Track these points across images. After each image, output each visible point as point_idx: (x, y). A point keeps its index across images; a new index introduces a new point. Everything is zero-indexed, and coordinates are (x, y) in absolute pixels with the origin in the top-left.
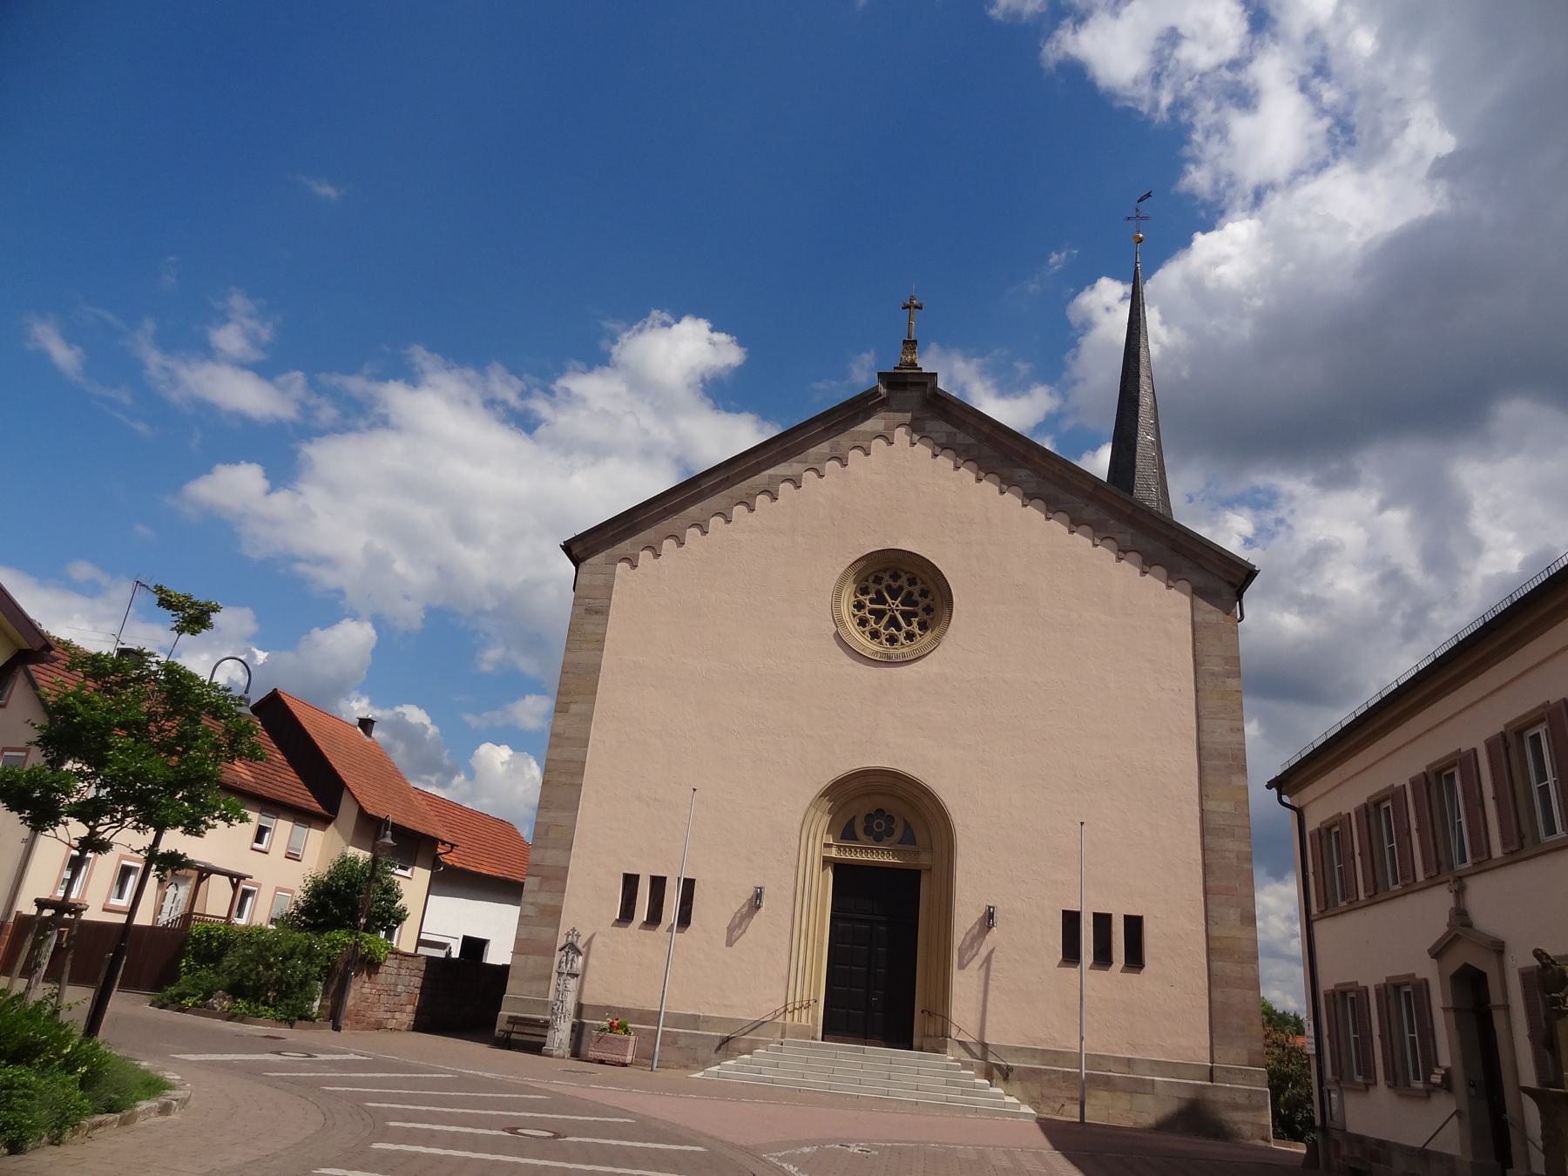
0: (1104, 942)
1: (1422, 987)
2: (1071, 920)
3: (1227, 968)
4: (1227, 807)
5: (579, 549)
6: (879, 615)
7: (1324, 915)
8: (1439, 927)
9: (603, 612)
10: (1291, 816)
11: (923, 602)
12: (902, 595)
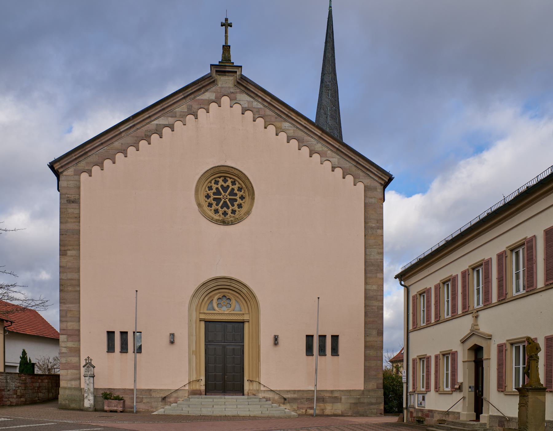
0: (321, 345)
1: (454, 354)
2: (309, 338)
3: (372, 353)
4: (375, 287)
5: (56, 167)
6: (218, 200)
7: (415, 329)
8: (466, 331)
9: (76, 201)
10: (402, 290)
11: (240, 194)
12: (226, 194)
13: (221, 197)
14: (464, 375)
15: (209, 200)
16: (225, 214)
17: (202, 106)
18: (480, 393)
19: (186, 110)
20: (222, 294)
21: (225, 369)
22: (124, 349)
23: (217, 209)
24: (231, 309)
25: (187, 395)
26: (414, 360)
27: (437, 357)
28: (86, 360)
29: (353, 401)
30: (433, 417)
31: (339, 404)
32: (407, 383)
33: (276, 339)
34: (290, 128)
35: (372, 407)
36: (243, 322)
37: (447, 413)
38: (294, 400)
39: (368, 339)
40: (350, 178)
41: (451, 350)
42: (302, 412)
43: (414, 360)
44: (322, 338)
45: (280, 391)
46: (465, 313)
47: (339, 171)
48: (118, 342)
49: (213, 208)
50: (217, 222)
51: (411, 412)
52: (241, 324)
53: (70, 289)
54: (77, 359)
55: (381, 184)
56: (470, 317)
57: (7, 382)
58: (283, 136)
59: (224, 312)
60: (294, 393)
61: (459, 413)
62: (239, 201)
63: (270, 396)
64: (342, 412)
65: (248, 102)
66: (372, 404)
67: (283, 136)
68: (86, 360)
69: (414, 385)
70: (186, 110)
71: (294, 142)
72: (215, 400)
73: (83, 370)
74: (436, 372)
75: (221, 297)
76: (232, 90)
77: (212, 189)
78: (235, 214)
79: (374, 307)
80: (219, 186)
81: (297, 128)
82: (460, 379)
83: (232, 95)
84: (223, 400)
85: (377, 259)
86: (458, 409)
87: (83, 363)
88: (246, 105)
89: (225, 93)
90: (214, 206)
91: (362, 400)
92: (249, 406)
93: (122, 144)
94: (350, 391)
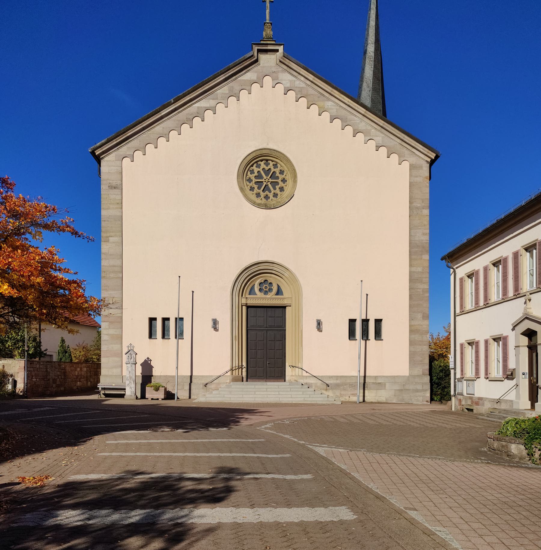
0: (363, 329)
7: (463, 313)
8: (519, 315)
13: (265, 184)
14: (519, 360)
15: (251, 184)
16: (267, 197)
17: (243, 87)
18: (535, 380)
19: (228, 92)
20: (264, 279)
22: (165, 335)
23: (259, 193)
26: (462, 345)
27: (486, 342)
28: (128, 347)
29: (397, 387)
30: (483, 405)
31: (383, 391)
32: (455, 369)
34: (333, 107)
35: (418, 394)
36: (284, 307)
37: (498, 401)
39: (413, 323)
40: (395, 157)
41: (502, 335)
42: (346, 399)
43: (462, 345)
44: (365, 322)
46: (517, 295)
47: (383, 151)
48: (159, 327)
49: (255, 192)
50: (259, 206)
51: (460, 401)
53: (112, 275)
54: (118, 346)
55: (427, 161)
56: (523, 300)
57: (47, 371)
58: (326, 116)
59: (260, 299)
61: (512, 401)
62: (281, 184)
63: (312, 382)
64: (386, 399)
65: (291, 81)
66: (417, 391)
67: (326, 116)
68: (128, 347)
69: (462, 371)
70: (228, 92)
71: (337, 122)
72: (256, 387)
73: (125, 357)
74: (487, 357)
75: (263, 281)
76: (274, 70)
77: (254, 173)
78: (277, 197)
79: (419, 290)
80: (261, 170)
81: (340, 106)
82: (512, 365)
83: (275, 74)
84: (265, 387)
85: (422, 240)
86: (512, 396)
87: (125, 350)
88: (288, 85)
89: (267, 73)
90: (256, 190)
91: (407, 387)
92: (291, 393)
93: (163, 128)
94: (394, 377)
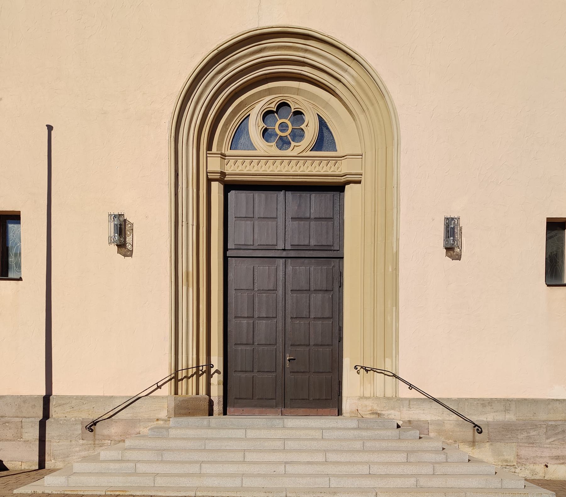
21: (277, 338)
24: (298, 148)
25: (163, 414)
33: (451, 229)
38: (507, 431)
45: (459, 401)
52: (316, 203)
60: (507, 410)
63: (428, 418)
72: (251, 434)
75: (273, 107)
84: (279, 433)
